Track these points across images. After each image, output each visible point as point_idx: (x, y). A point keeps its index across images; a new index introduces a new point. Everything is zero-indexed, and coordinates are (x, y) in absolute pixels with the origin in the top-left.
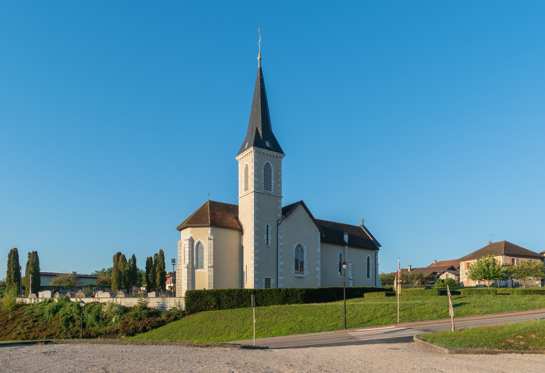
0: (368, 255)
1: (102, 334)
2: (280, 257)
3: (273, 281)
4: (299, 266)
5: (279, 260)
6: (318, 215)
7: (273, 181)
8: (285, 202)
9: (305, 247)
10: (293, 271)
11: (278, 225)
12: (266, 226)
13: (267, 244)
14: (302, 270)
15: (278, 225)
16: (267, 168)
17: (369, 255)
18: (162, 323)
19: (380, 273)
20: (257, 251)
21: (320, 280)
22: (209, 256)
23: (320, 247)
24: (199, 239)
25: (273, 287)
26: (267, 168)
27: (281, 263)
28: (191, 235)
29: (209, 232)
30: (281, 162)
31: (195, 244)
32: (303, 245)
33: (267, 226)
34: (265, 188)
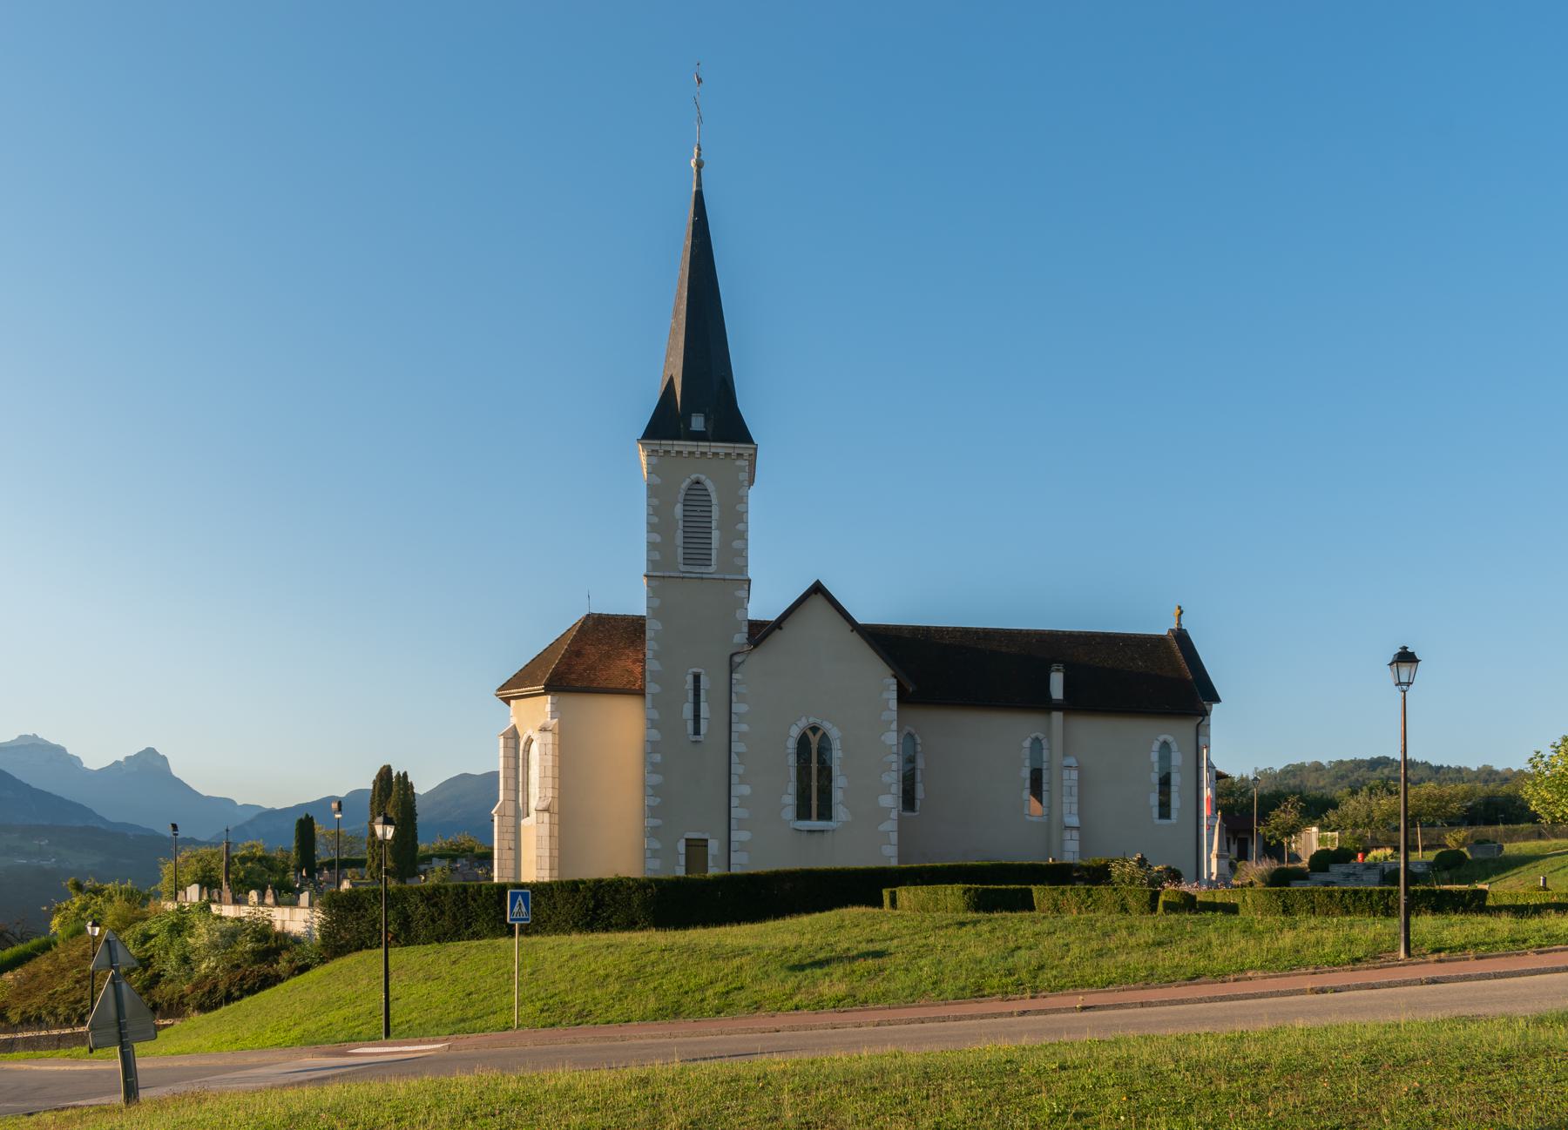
0: (1162, 738)
3: (714, 847)
4: (814, 797)
5: (734, 779)
6: (872, 605)
7: (715, 534)
10: (790, 812)
11: (732, 668)
12: (690, 679)
13: (697, 732)
14: (826, 813)
15: (732, 668)
16: (696, 496)
17: (1170, 738)
21: (894, 837)
22: (543, 777)
23: (894, 726)
25: (714, 871)
26: (696, 496)
27: (741, 790)
29: (548, 708)
33: (697, 678)
34: (687, 560)
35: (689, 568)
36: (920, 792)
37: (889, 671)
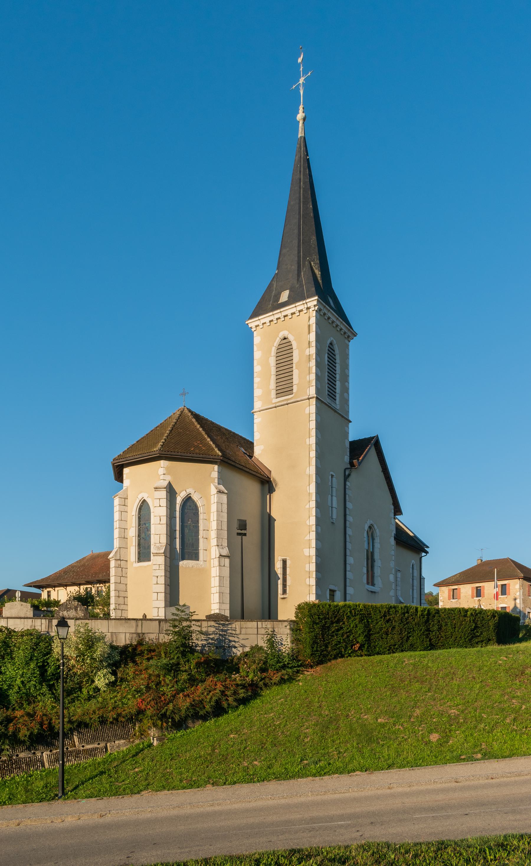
1: (86, 725)
8: (355, 433)
15: (346, 478)
18: (253, 691)
19: (426, 591)
24: (189, 491)
28: (169, 478)
29: (215, 475)
30: (348, 346)
31: (179, 500)
32: (376, 527)
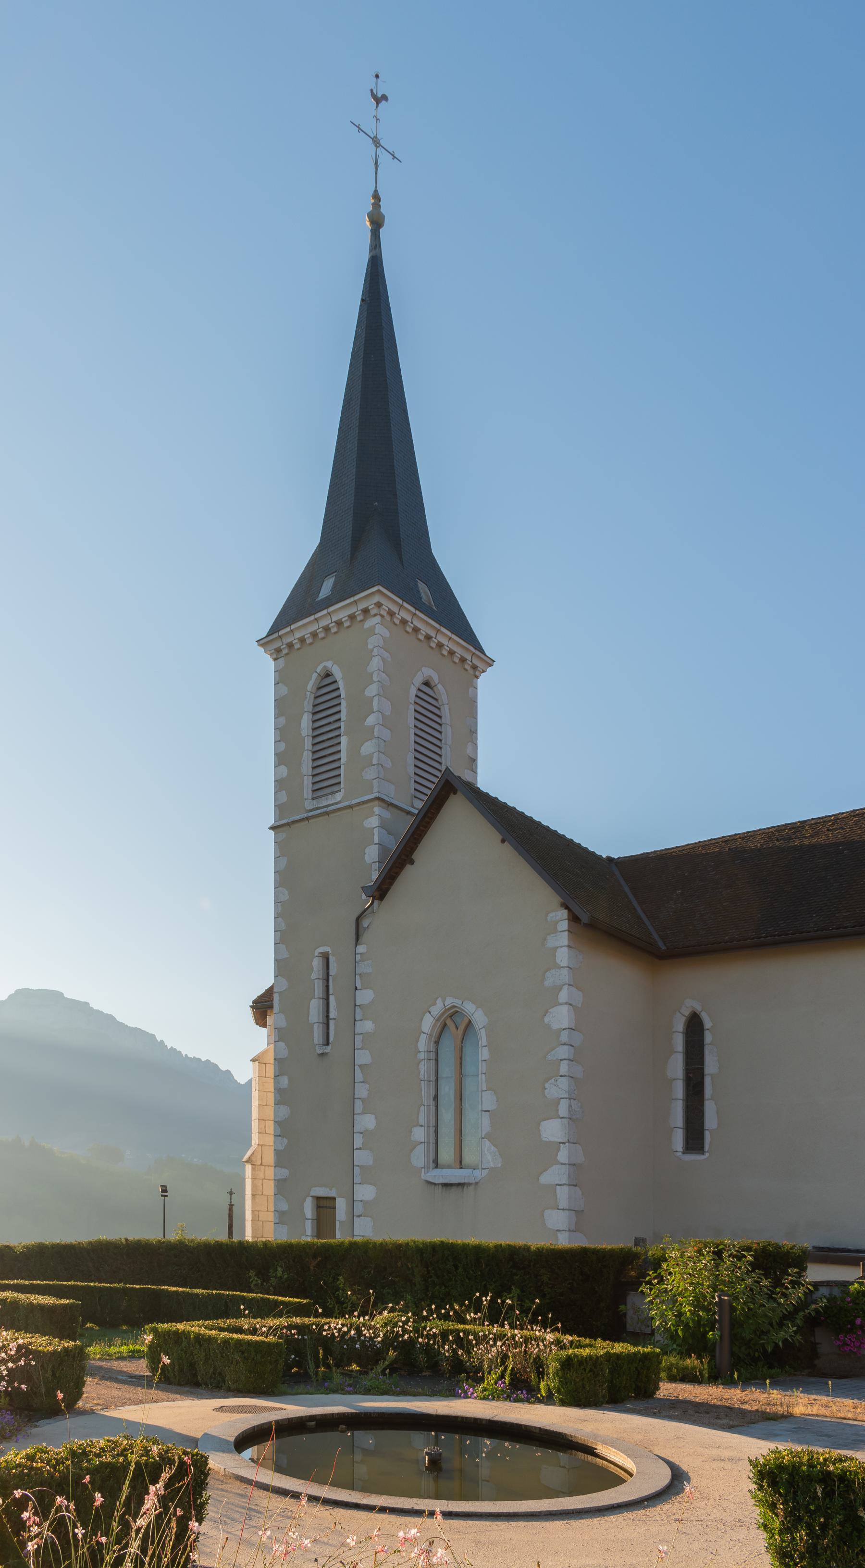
2: (362, 1091)
3: (341, 1205)
9: (708, 1023)
12: (317, 963)
16: (326, 701)
20: (285, 1081)
32: (469, 1008)
33: (326, 958)
34: (318, 791)
35: (315, 804)
36: (711, 1120)
37: (556, 899)
